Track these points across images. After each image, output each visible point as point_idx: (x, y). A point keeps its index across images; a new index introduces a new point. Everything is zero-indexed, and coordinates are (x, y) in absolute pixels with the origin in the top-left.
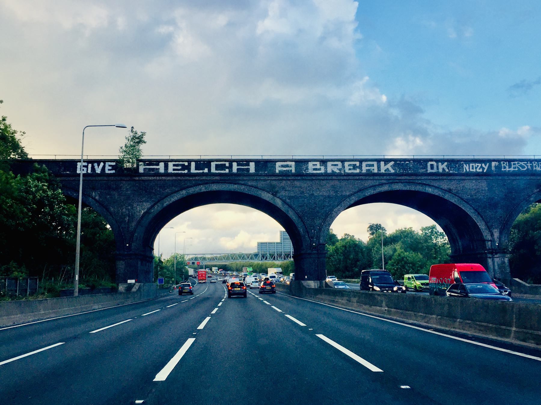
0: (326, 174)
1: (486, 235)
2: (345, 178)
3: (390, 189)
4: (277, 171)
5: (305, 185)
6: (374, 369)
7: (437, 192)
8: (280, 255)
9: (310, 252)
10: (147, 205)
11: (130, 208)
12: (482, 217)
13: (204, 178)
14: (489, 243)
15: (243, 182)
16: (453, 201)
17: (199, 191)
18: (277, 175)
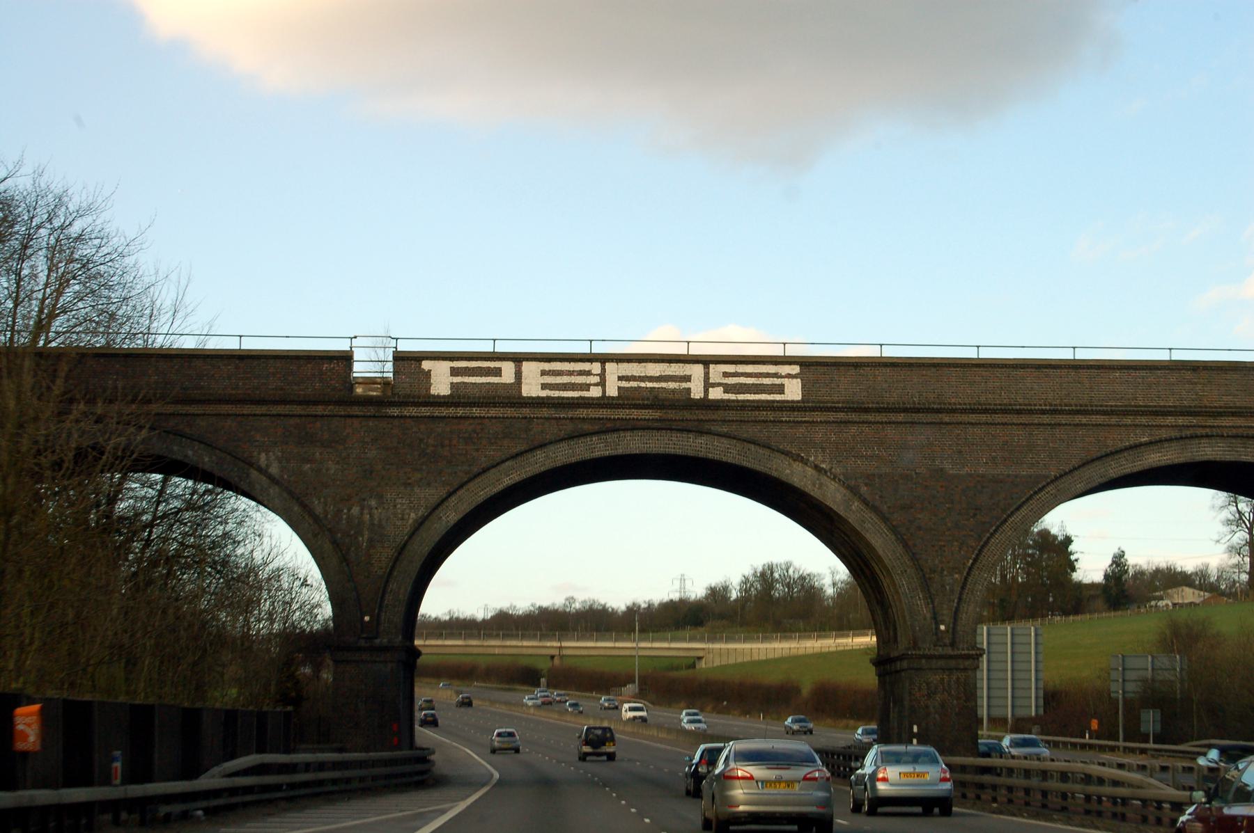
10: (430, 495)
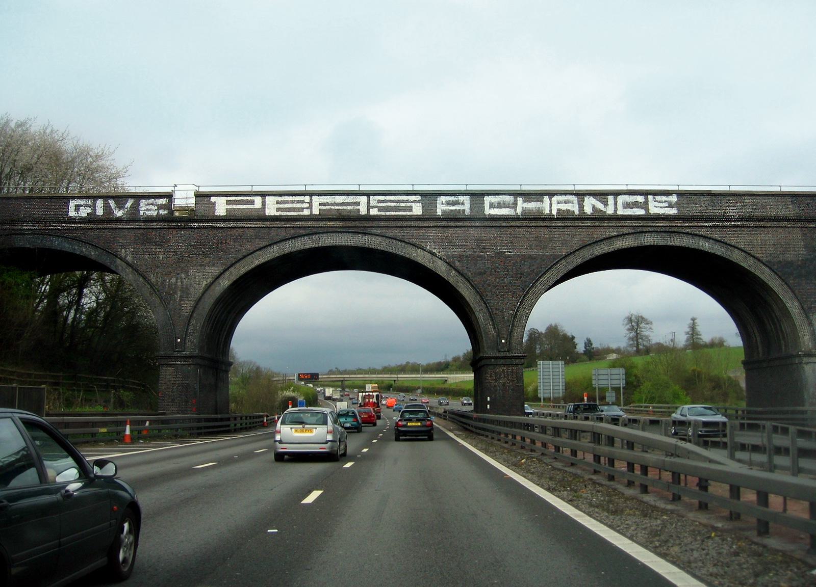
0: (582, 217)
2: (559, 223)
4: (439, 213)
6: (269, 531)
7: (718, 250)
11: (183, 276)
12: (793, 292)
15: (379, 231)
17: (302, 247)
18: (439, 219)
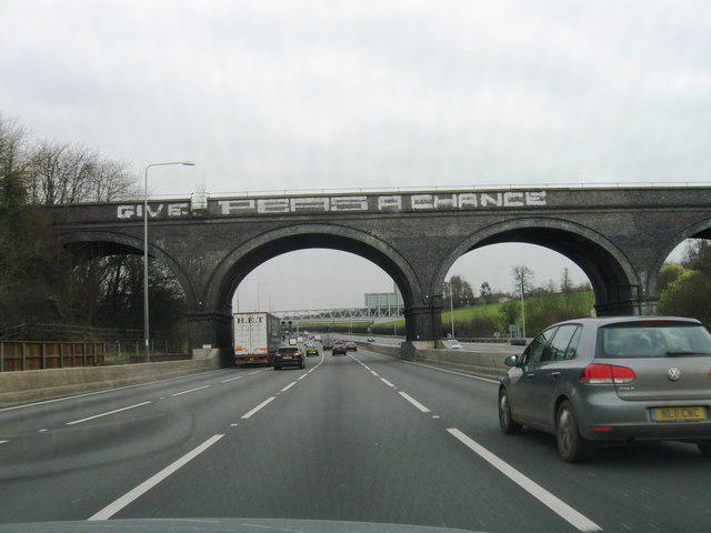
0: (480, 209)
1: (633, 281)
2: (463, 213)
3: (536, 225)
5: (414, 223)
8: (384, 311)
9: (424, 313)
10: (222, 254)
13: (290, 218)
14: (635, 289)
16: (593, 239)
18: (379, 213)
